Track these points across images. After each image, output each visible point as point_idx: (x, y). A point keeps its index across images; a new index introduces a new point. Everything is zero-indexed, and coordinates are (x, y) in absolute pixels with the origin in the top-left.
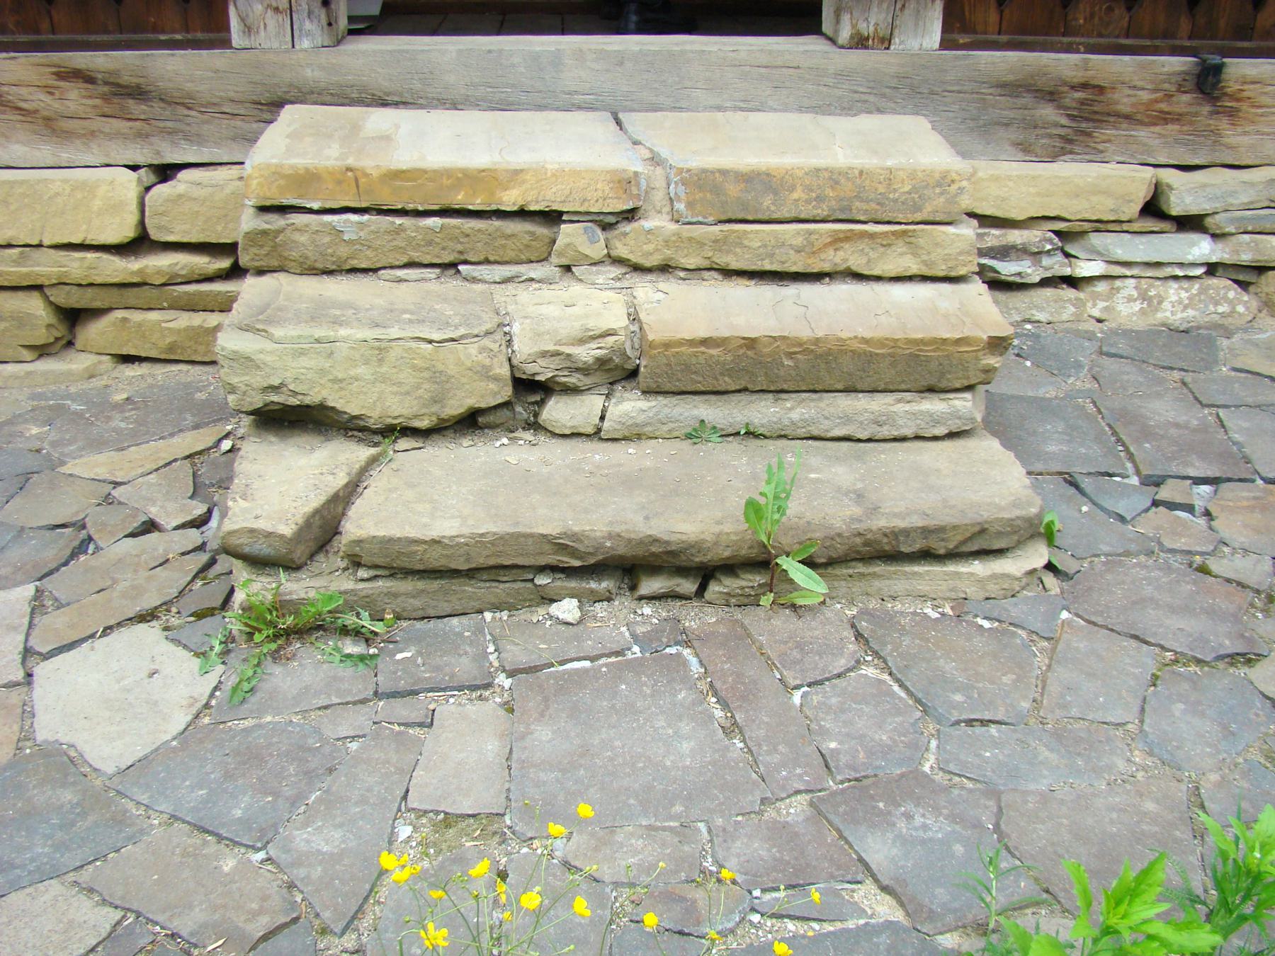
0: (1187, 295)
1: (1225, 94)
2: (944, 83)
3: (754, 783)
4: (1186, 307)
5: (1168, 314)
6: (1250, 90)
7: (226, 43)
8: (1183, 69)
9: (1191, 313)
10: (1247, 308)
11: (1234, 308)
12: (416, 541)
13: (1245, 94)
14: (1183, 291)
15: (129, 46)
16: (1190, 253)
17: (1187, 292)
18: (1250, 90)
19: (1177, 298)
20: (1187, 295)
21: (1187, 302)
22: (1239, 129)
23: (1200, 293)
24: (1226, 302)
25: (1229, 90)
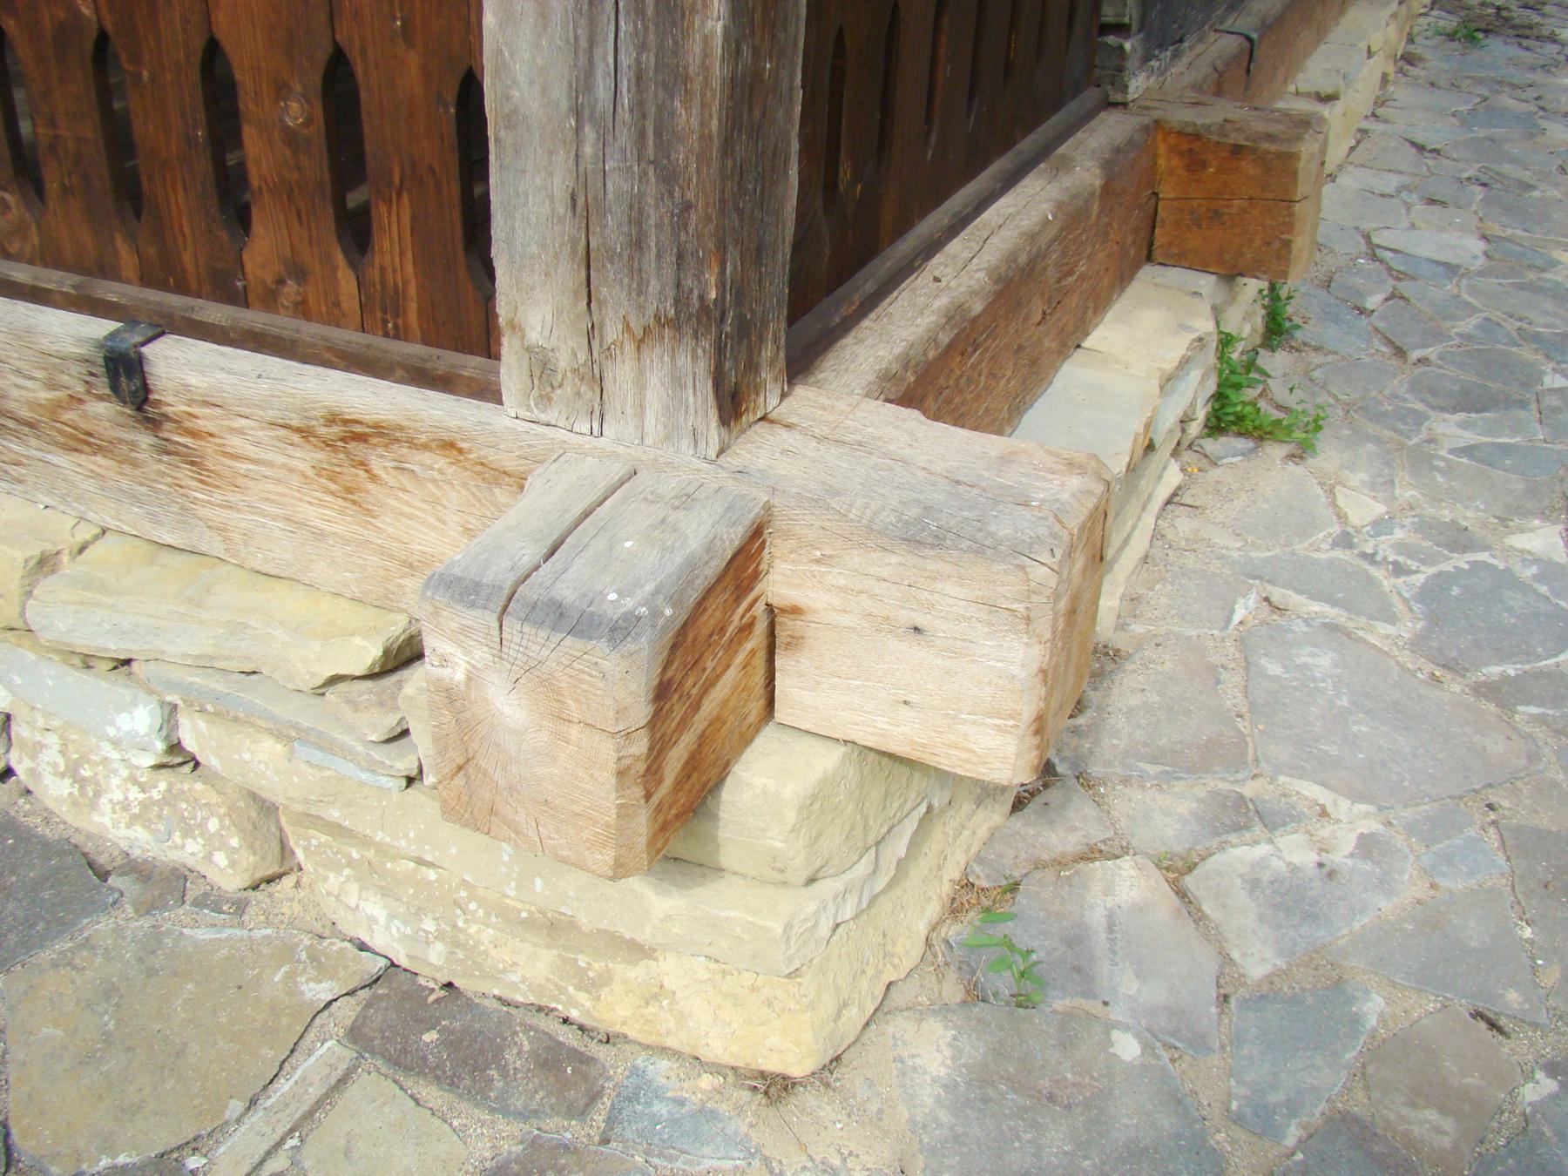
0: (141, 796)
1: (166, 417)
2: (872, 490)
3: (330, 1015)
4: (134, 819)
5: (107, 821)
6: (207, 421)
7: (488, 392)
8: (79, 351)
9: (140, 833)
10: (233, 864)
11: (211, 854)
12: (685, 625)
13: (201, 424)
14: (136, 788)
15: (422, 377)
16: (112, 723)
17: (143, 791)
18: (205, 418)
19: (121, 798)
20: (141, 796)
21: (136, 810)
22: (218, 497)
23: (164, 802)
24: (202, 835)
25: (170, 409)
